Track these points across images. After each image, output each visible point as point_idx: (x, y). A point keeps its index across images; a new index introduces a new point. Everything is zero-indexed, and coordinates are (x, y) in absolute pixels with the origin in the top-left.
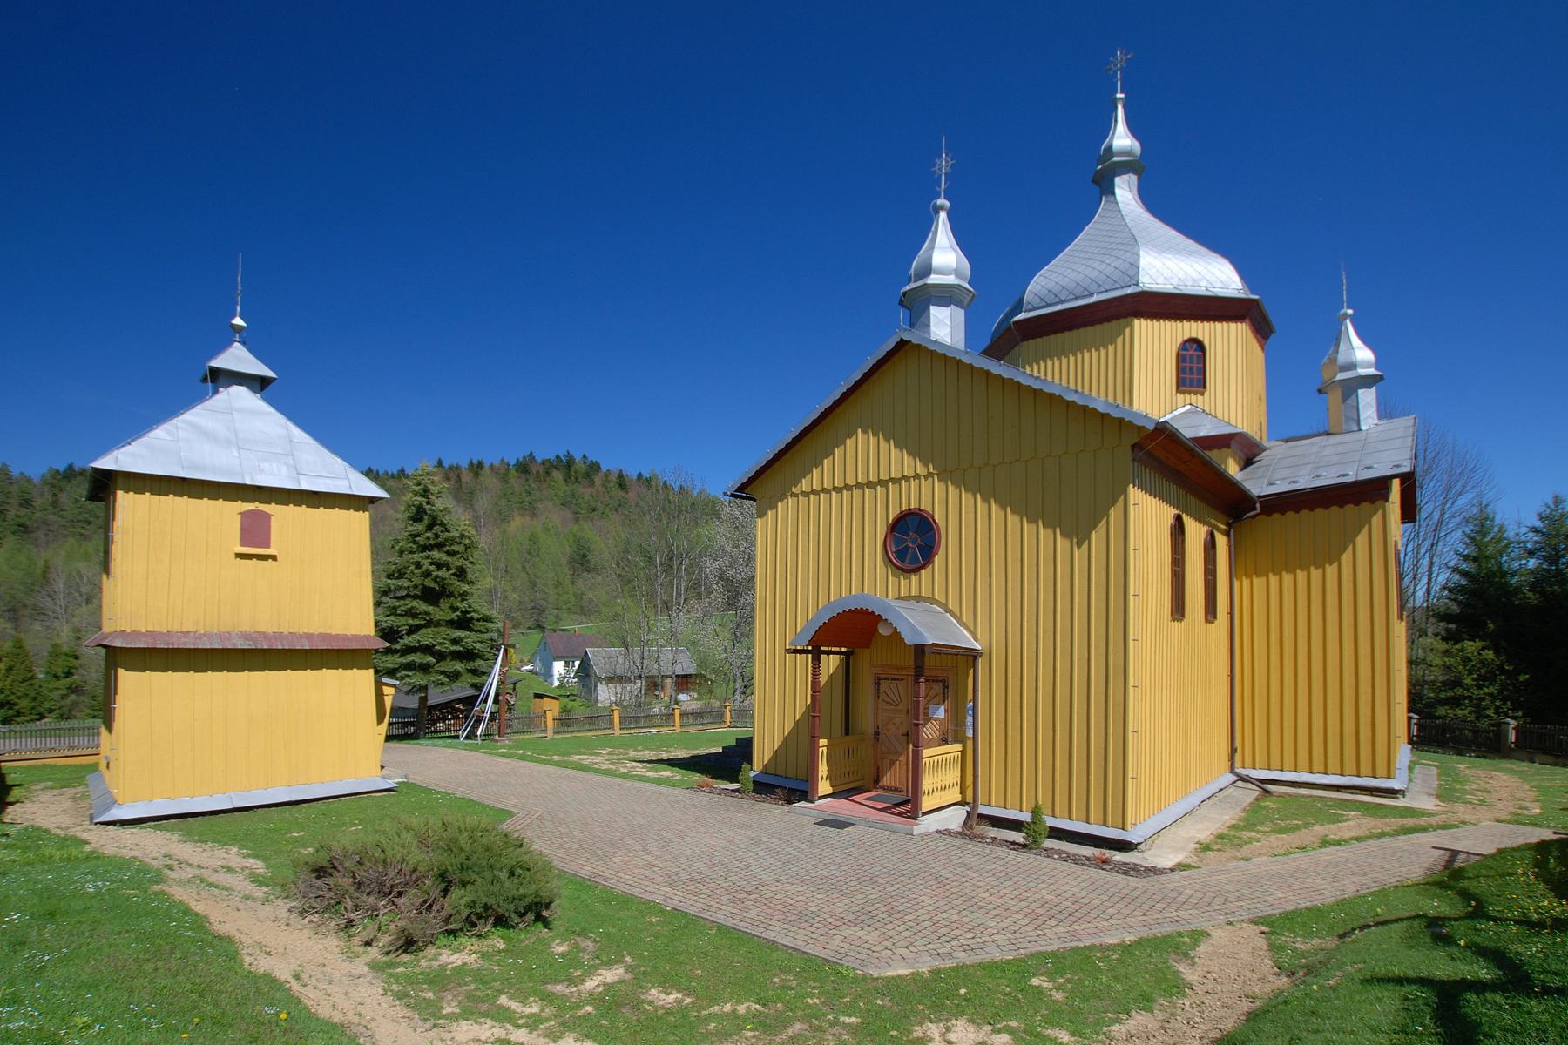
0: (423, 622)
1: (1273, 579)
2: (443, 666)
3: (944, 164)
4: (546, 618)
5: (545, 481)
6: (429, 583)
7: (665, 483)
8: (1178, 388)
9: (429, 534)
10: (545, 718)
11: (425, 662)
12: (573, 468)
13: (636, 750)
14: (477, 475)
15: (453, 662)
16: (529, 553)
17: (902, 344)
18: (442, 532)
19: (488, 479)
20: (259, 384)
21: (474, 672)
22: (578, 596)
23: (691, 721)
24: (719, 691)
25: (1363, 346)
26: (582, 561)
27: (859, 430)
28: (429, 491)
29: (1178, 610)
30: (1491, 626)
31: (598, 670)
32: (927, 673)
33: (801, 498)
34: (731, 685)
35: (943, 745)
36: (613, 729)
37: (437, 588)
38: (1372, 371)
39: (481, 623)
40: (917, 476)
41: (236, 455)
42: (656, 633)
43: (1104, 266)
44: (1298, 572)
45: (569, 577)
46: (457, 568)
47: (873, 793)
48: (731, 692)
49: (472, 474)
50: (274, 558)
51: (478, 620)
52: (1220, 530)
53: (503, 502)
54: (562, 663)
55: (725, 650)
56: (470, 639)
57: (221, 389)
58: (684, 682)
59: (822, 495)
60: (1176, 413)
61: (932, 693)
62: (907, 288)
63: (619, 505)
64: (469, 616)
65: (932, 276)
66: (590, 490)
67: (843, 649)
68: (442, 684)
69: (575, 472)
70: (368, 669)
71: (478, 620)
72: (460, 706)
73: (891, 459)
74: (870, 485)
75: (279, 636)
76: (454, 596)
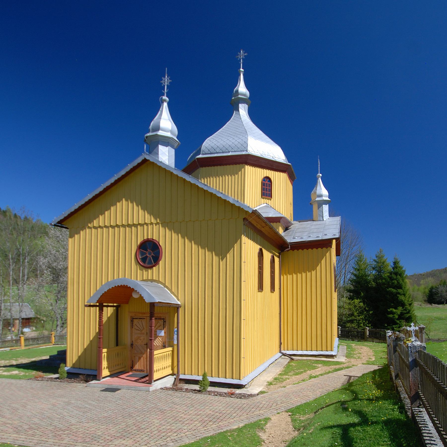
3: (166, 81)
8: (262, 196)
17: (145, 161)
24: (48, 326)
27: (124, 199)
29: (261, 287)
30: (362, 294)
32: (156, 315)
33: (93, 230)
34: (55, 322)
35: (164, 348)
38: (327, 199)
40: (152, 224)
47: (130, 373)
48: (55, 326)
55: (52, 305)
58: (27, 322)
59: (104, 229)
61: (158, 325)
62: (148, 135)
65: (160, 131)
67: (115, 304)
74: (129, 226)
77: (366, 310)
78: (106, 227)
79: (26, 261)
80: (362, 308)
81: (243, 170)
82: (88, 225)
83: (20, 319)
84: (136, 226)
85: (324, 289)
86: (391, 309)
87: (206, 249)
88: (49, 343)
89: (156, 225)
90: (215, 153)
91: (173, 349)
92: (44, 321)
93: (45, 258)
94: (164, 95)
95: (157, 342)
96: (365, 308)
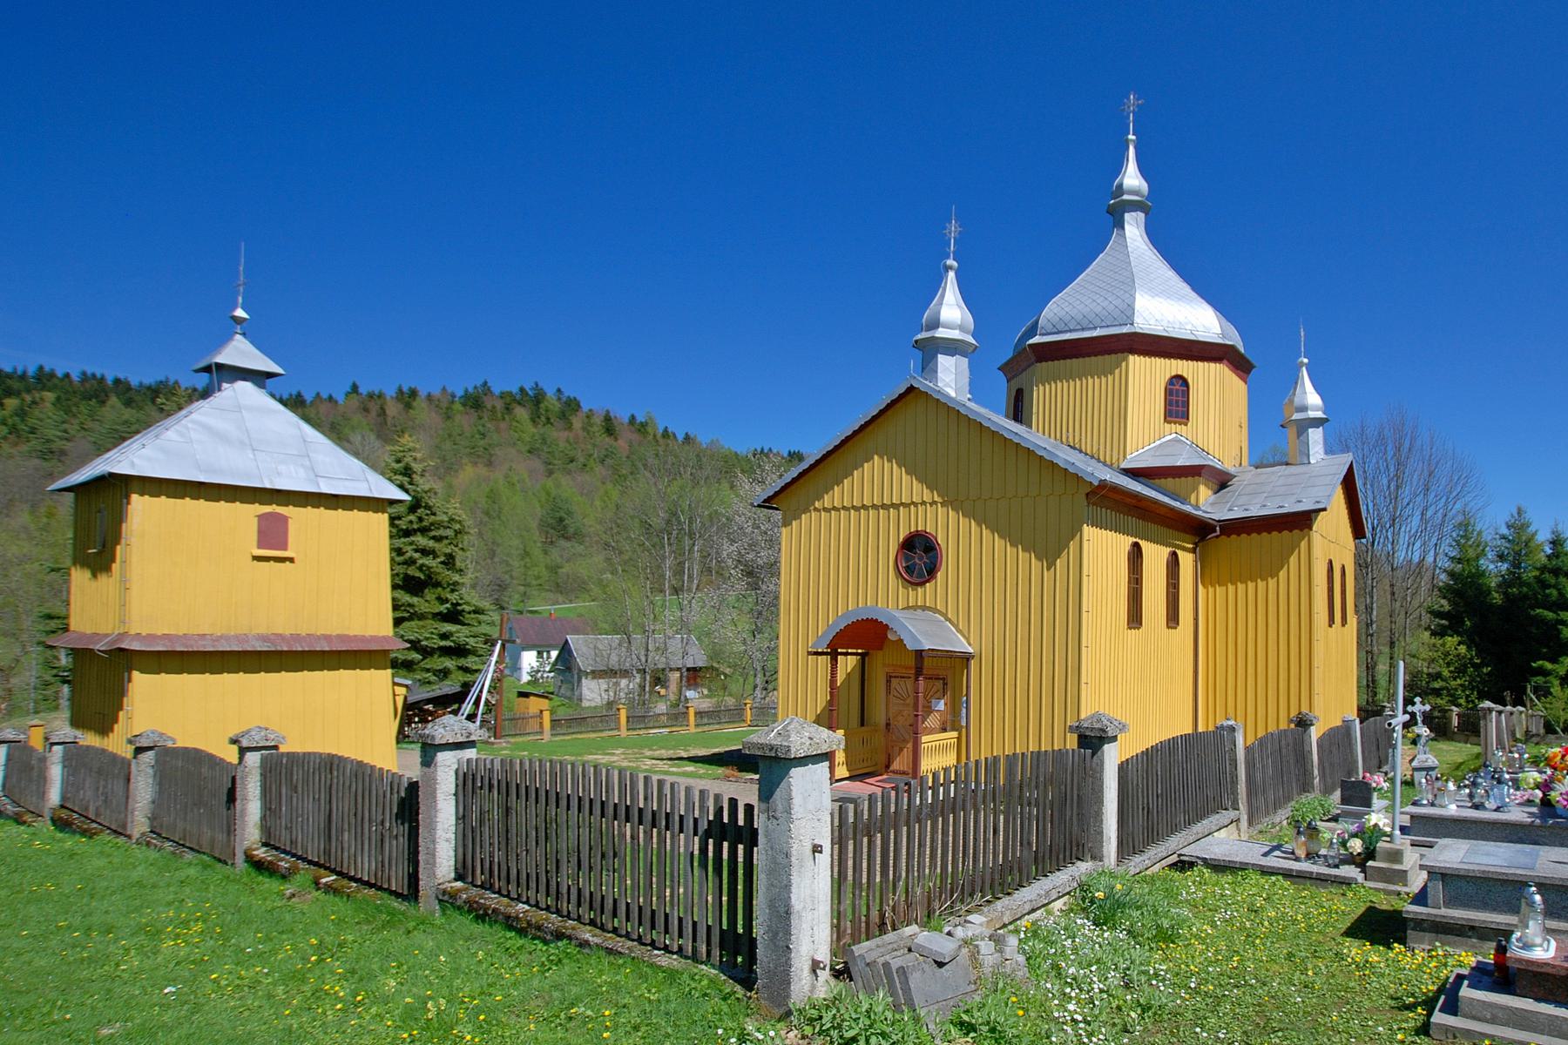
0: (406, 615)
1: (1231, 588)
2: (428, 663)
3: (953, 229)
4: (510, 597)
5: (504, 419)
6: (413, 571)
7: (666, 430)
8: (1165, 418)
9: (412, 517)
10: (542, 718)
11: (410, 658)
12: (542, 405)
13: (651, 750)
14: (408, 406)
15: (442, 659)
16: (487, 513)
17: (911, 389)
18: (427, 515)
19: (421, 408)
20: (259, 378)
21: (466, 670)
22: (553, 569)
23: (705, 721)
24: (734, 687)
25: (1314, 391)
26: (559, 526)
27: (876, 457)
28: (410, 469)
29: (1135, 618)
30: (1468, 623)
31: (583, 659)
32: (925, 672)
33: (823, 513)
34: (751, 679)
36: (618, 729)
37: (423, 577)
38: (1319, 414)
39: (473, 616)
40: (923, 503)
41: (251, 456)
42: (663, 623)
43: (1106, 303)
44: (1249, 582)
45: (539, 545)
46: (446, 555)
47: (885, 777)
48: (749, 687)
49: (401, 406)
50: (291, 560)
51: (469, 613)
52: (1184, 549)
53: (448, 445)
54: (534, 654)
55: (744, 642)
56: (460, 633)
57: (225, 385)
58: (693, 676)
59: (842, 512)
60: (1164, 440)
61: (934, 689)
62: (919, 337)
63: (606, 456)
64: (459, 608)
65: (940, 329)
66: (566, 433)
67: (860, 651)
68: (429, 683)
69: (547, 411)
70: (385, 669)
71: (469, 613)
72: (430, 707)
73: (902, 484)
74: (884, 506)
75: (296, 637)
76: (441, 586)
77: (1474, 665)
78: (844, 508)
79: (696, 548)
80: (1463, 657)
81: (1124, 364)
82: (814, 504)
83: (684, 670)
84: (896, 506)
85: (1294, 620)
86: (1541, 662)
87: (1020, 547)
88: (738, 722)
89: (931, 506)
90: (1066, 332)
91: (960, 734)
92: (726, 675)
93: (733, 541)
94: (948, 257)
95: (932, 721)
96: (1471, 659)
